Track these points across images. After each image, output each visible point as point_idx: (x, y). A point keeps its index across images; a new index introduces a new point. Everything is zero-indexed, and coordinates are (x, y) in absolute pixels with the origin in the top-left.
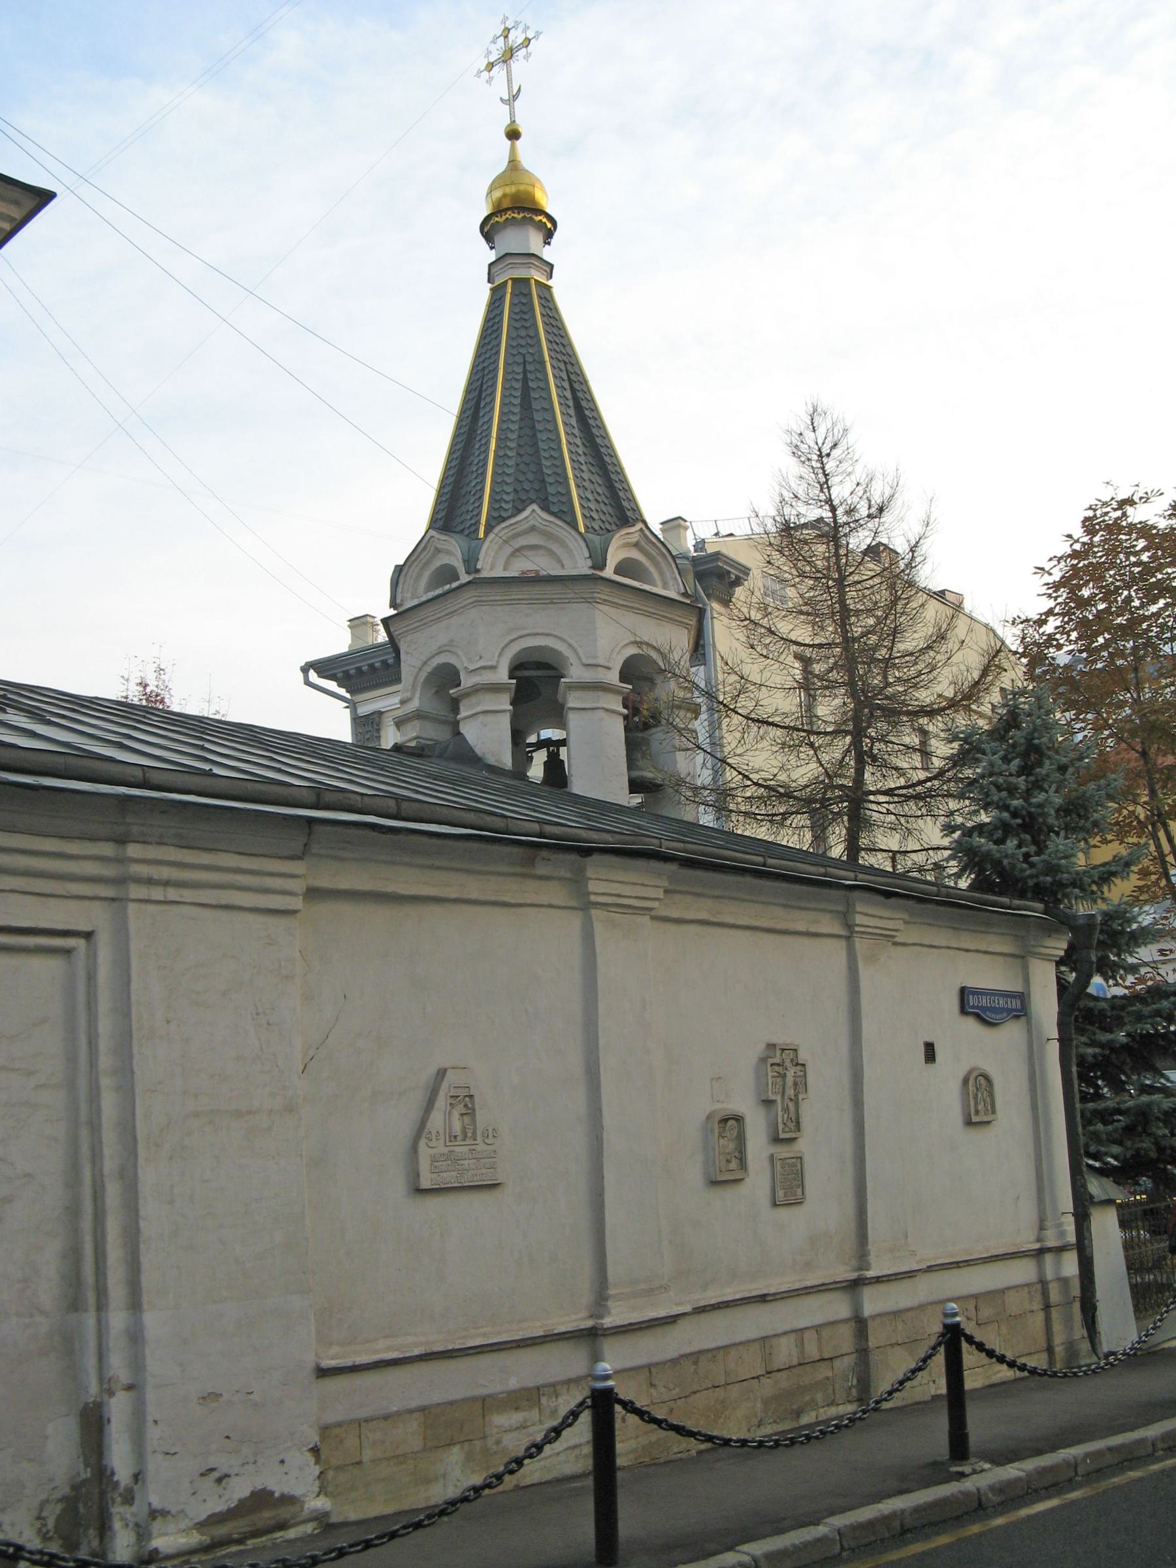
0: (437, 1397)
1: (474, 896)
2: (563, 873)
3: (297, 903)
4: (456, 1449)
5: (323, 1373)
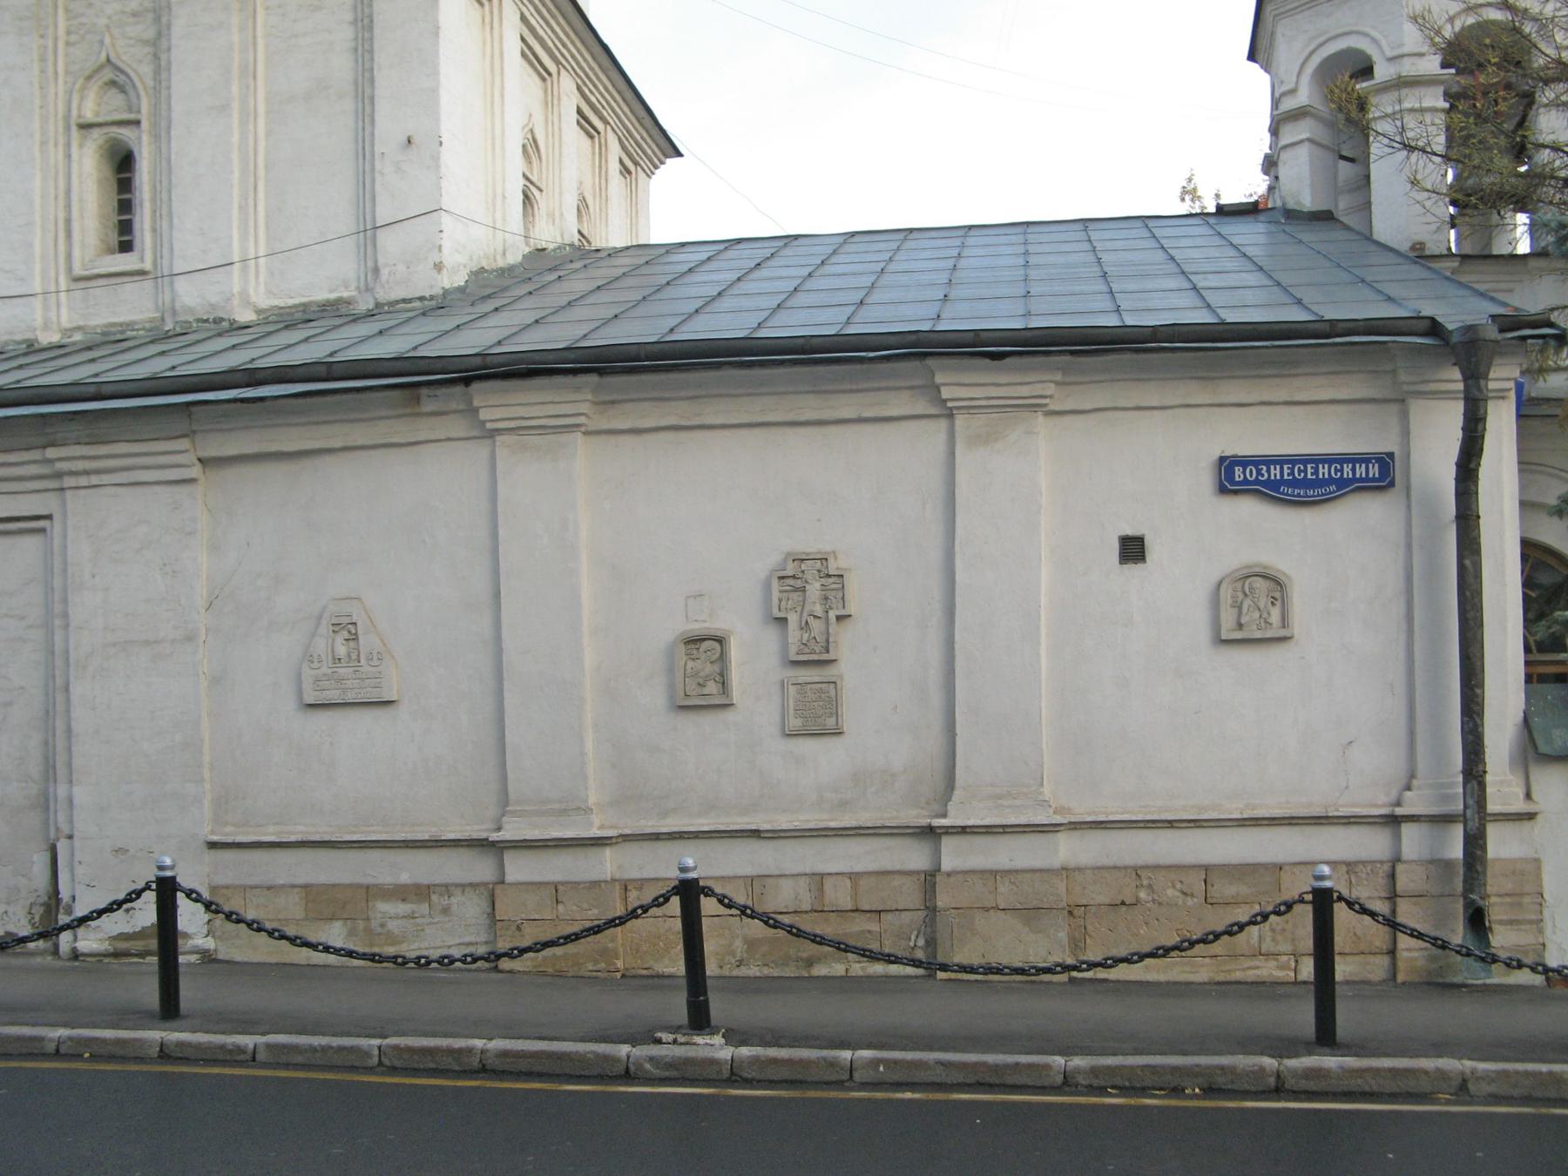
0: (323, 878)
1: (360, 442)
2: (453, 406)
3: (196, 471)
4: (338, 924)
5: (213, 845)
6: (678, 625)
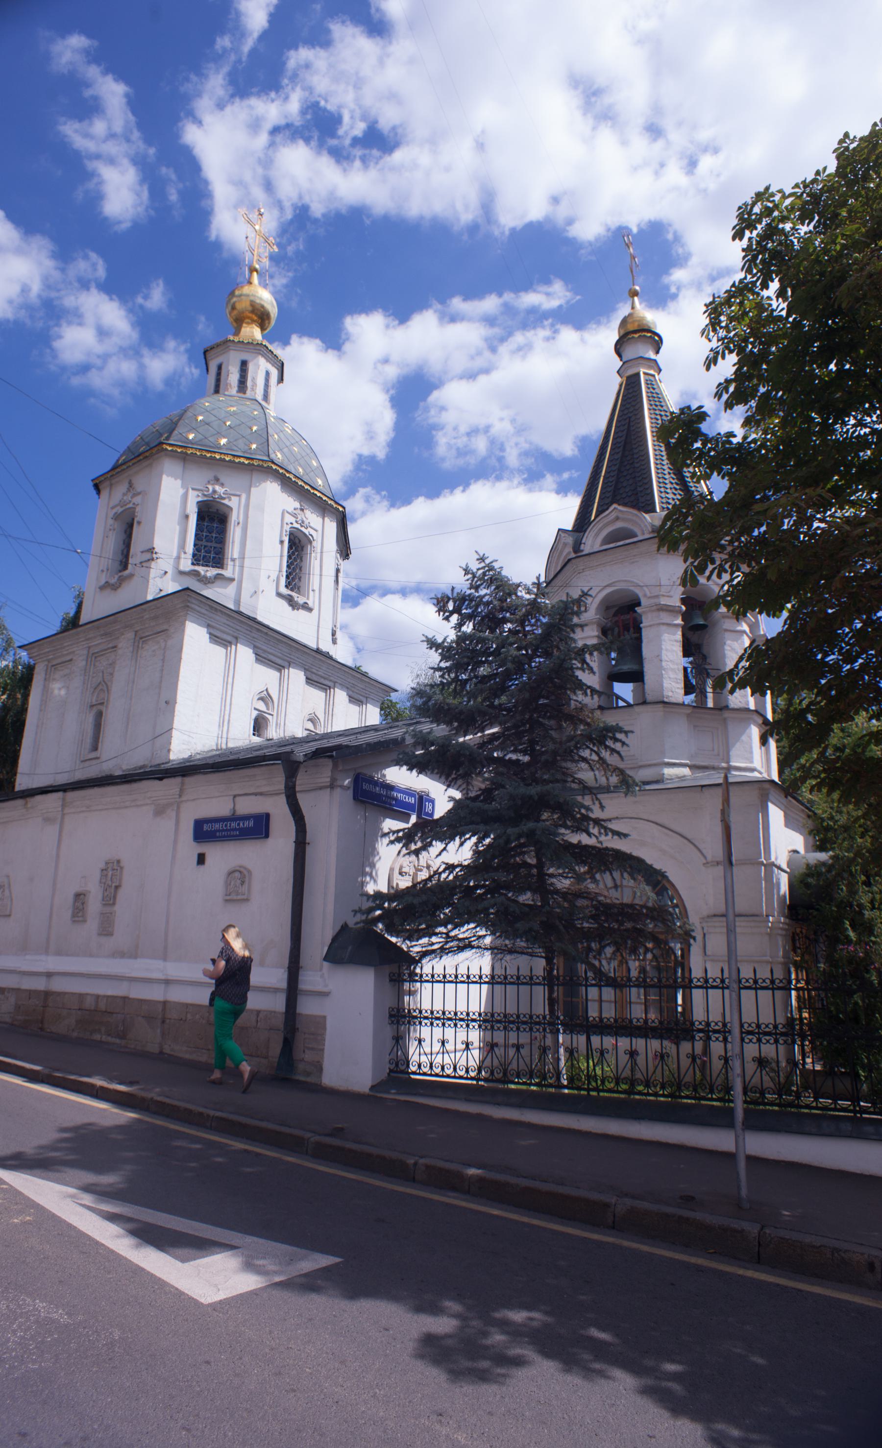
6: (78, 889)
